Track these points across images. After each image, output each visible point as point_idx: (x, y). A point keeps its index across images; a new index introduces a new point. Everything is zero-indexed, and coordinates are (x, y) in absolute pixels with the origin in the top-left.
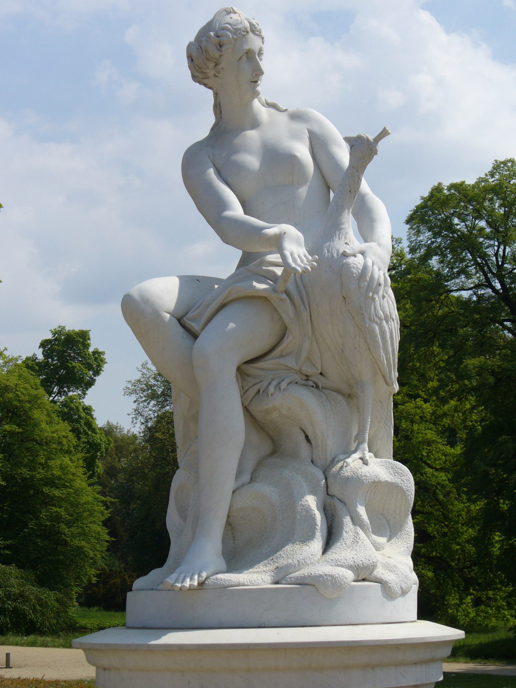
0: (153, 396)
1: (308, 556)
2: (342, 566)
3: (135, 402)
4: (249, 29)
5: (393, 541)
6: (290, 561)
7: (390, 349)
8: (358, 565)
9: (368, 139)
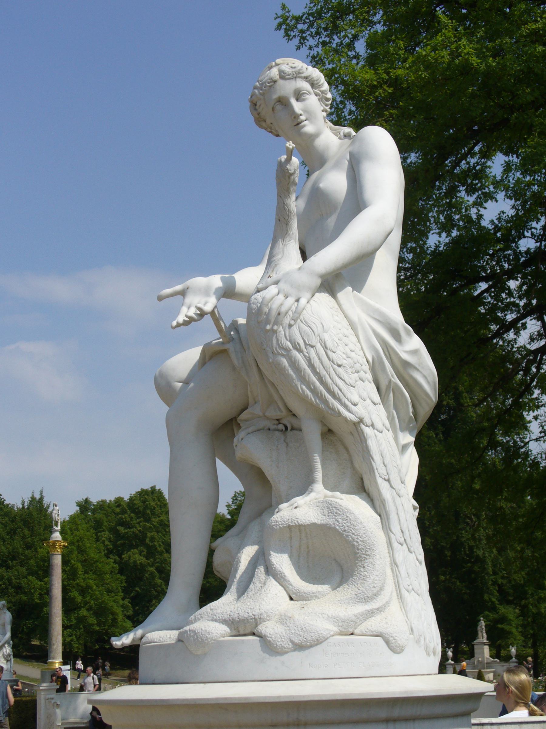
2: (216, 621)
8: (233, 619)
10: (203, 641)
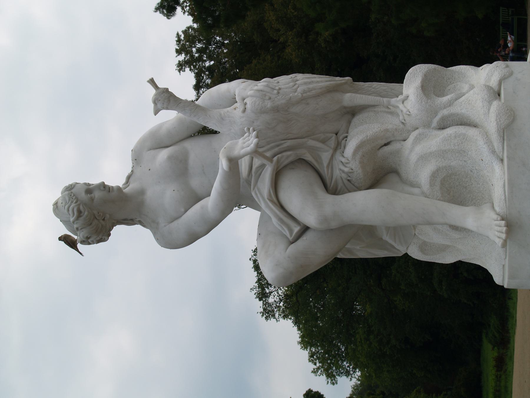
2: (489, 110)
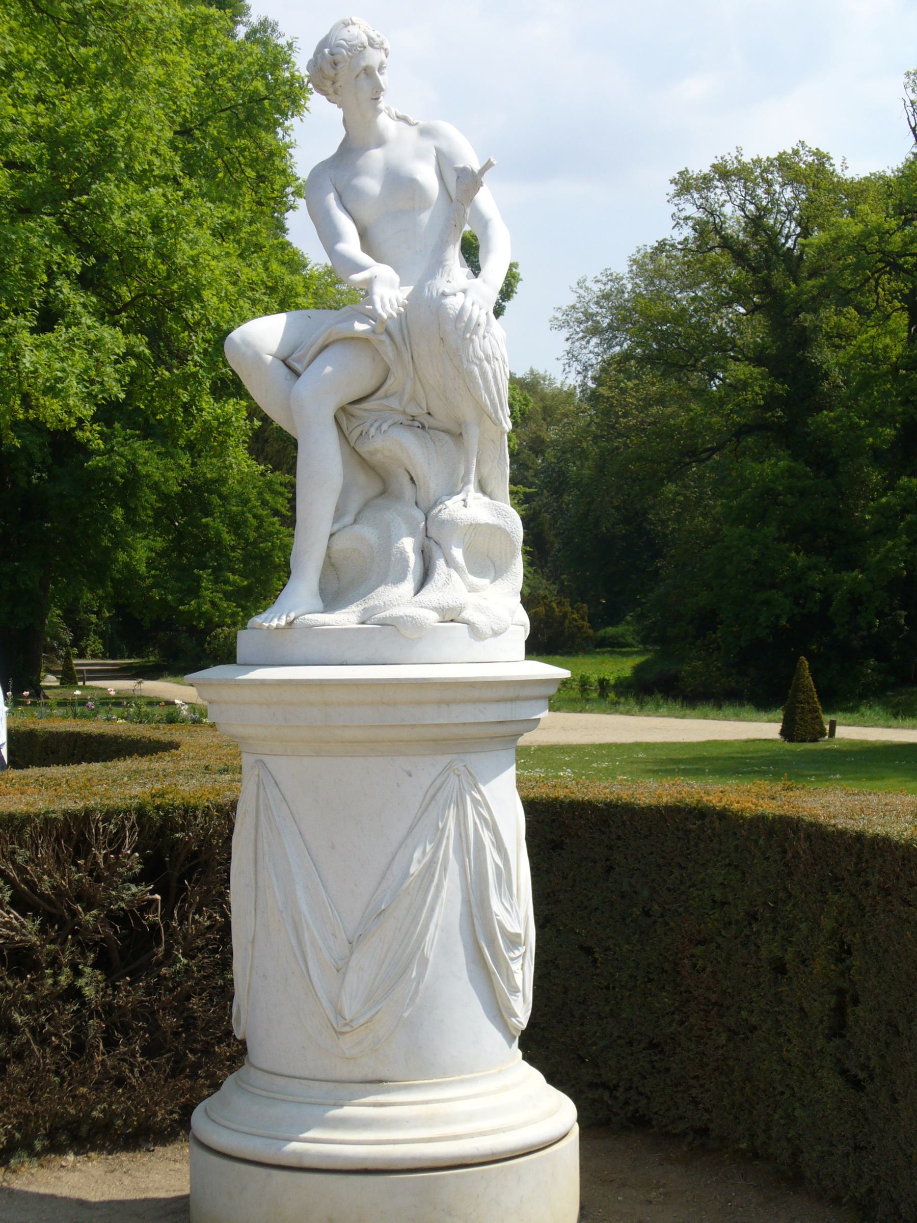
0: (595, 331)
1: (397, 598)
2: (426, 608)
3: (567, 339)
4: (366, 44)
5: (497, 582)
6: (377, 602)
7: (494, 390)
9: (473, 171)
10: (422, 626)
